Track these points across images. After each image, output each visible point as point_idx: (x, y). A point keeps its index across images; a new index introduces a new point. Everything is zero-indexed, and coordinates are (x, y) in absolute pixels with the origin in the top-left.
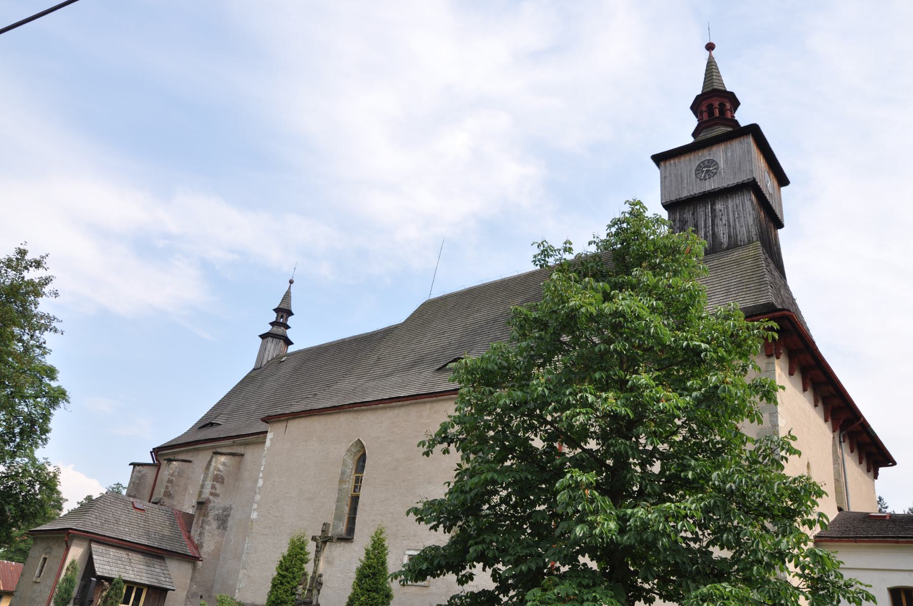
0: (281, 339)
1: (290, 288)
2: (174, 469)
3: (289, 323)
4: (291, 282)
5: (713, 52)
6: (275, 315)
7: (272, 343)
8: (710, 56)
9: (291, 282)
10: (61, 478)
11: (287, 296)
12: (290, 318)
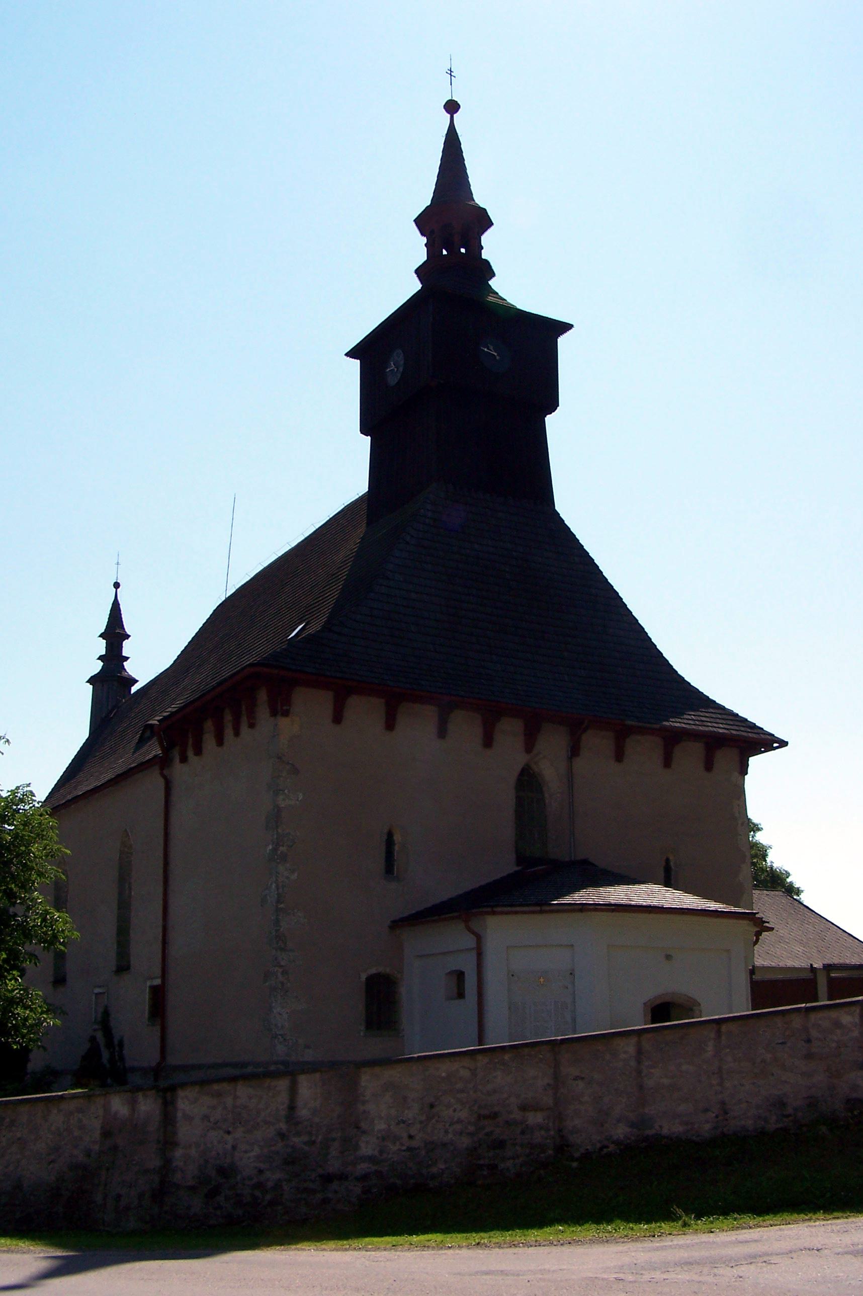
4: (117, 585)
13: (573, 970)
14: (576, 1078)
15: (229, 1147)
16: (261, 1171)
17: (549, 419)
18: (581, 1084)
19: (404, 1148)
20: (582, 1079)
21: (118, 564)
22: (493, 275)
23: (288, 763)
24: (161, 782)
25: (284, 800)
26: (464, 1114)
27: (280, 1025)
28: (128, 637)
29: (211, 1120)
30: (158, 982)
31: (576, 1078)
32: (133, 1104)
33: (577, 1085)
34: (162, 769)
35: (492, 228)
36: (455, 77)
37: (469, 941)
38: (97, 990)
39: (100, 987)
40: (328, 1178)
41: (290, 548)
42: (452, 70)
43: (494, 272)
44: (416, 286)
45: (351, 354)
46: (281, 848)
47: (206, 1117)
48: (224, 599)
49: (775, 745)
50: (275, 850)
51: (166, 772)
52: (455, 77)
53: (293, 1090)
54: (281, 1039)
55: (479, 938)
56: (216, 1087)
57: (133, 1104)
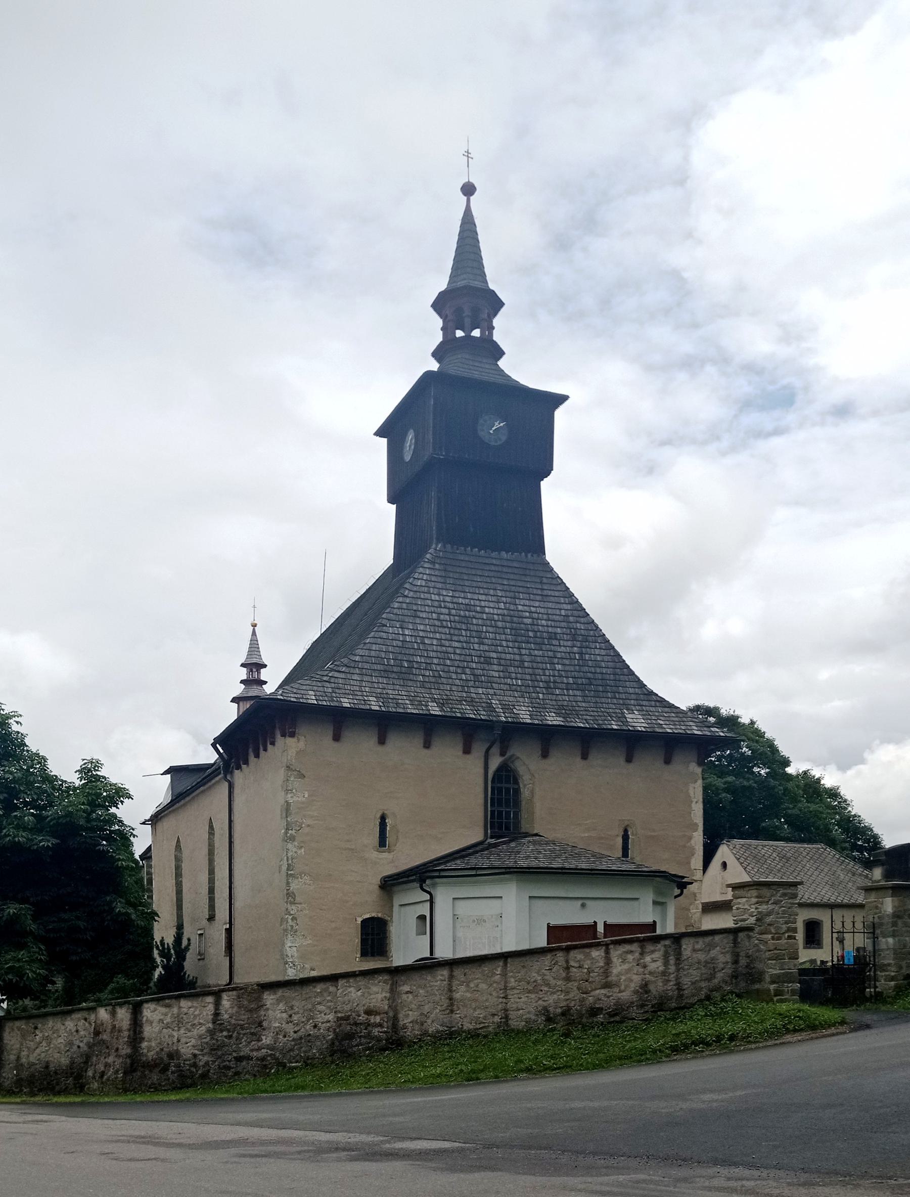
3: (263, 678)
5: (472, 198)
14: (407, 992)
15: (175, 1040)
16: (195, 1056)
17: (542, 482)
18: (411, 996)
19: (291, 1039)
20: (411, 993)
22: (501, 353)
23: (296, 770)
24: (226, 784)
25: (292, 797)
26: (331, 1017)
27: (290, 955)
29: (165, 1022)
30: (228, 926)
31: (407, 992)
32: (113, 1014)
33: (408, 997)
35: (431, 304)
36: (472, 158)
38: (199, 932)
40: (239, 1059)
41: (351, 603)
42: (469, 152)
43: (503, 351)
45: (380, 433)
46: (290, 832)
47: (161, 1021)
50: (286, 833)
52: (472, 158)
53: (217, 1004)
54: (291, 965)
56: (167, 1001)
57: (113, 1014)
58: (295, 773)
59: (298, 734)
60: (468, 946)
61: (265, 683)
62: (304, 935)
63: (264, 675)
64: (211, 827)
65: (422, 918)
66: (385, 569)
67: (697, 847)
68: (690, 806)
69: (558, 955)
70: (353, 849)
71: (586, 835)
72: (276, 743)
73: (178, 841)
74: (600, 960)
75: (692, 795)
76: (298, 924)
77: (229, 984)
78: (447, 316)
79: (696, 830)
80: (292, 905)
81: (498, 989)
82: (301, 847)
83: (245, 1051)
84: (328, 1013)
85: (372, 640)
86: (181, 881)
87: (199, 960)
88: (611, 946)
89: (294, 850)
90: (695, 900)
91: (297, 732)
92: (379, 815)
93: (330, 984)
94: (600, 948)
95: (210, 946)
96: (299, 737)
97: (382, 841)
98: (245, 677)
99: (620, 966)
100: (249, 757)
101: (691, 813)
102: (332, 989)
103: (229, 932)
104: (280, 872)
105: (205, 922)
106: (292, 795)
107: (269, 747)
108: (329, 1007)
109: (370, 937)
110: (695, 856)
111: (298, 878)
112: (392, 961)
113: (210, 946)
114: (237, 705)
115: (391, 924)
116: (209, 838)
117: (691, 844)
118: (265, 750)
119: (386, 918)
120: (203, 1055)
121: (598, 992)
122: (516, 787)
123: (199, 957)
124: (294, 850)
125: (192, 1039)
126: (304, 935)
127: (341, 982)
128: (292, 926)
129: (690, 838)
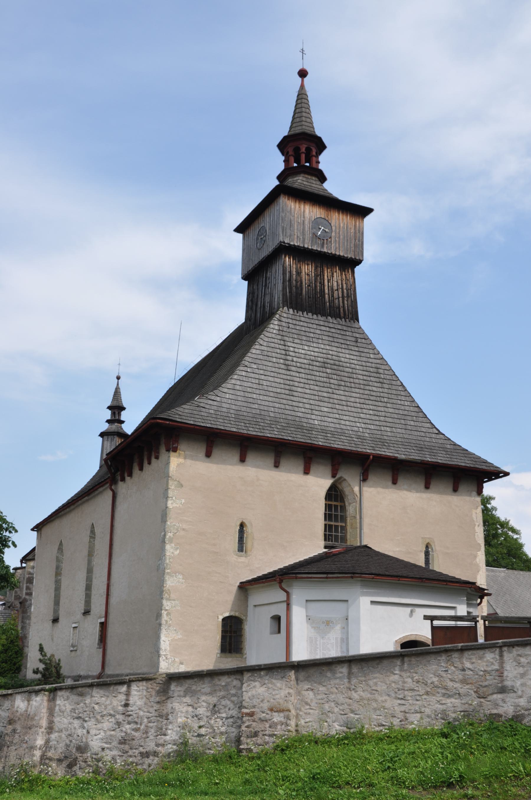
0: (115, 435)
1: (118, 384)
2: (19, 576)
3: (122, 418)
4: (118, 378)
5: (305, 79)
6: (109, 412)
7: (108, 440)
8: (302, 86)
9: (118, 378)
10: (525, 546)
11: (117, 393)
12: (123, 413)
13: (348, 616)
21: (119, 364)
24: (110, 493)
28: (124, 409)
29: (77, 711)
30: (103, 620)
34: (111, 485)
37: (283, 596)
38: (74, 625)
39: (75, 623)
44: (277, 183)
48: (173, 384)
49: (501, 475)
51: (113, 487)
53: (128, 694)
55: (288, 594)
56: (80, 689)
58: (176, 483)
59: (180, 449)
60: (318, 646)
61: (123, 422)
62: (175, 630)
63: (124, 415)
64: (93, 532)
65: (277, 619)
66: (231, 332)
67: (481, 565)
68: (474, 528)
69: (453, 656)
70: (218, 553)
71: (398, 549)
72: (160, 457)
73: (61, 544)
74: (494, 663)
75: (475, 519)
76: (171, 619)
77: (99, 676)
78: (288, 153)
79: (479, 550)
80: (168, 601)
81: (397, 690)
82: (177, 548)
83: (151, 746)
84: (231, 708)
85: (239, 377)
86: (60, 580)
87: (71, 651)
88: (505, 649)
89: (172, 550)
90: (482, 612)
91: (178, 448)
92: (239, 523)
93: (235, 677)
94: (494, 649)
95: (83, 639)
96: (180, 452)
97: (241, 546)
98: (109, 418)
99: (515, 669)
100: (133, 470)
101: (475, 535)
102: (236, 683)
103: (103, 626)
104: (158, 570)
105: (79, 616)
106: (172, 501)
107: (153, 460)
108: (233, 702)
109: (228, 634)
110: (480, 572)
111: (173, 576)
112: (246, 658)
113: (83, 639)
114: (102, 438)
115: (245, 623)
116: (90, 542)
117: (476, 562)
118: (149, 463)
119: (241, 617)
120: (110, 749)
121: (495, 696)
122: (342, 504)
123: (72, 649)
124: (172, 550)
125: (102, 731)
126: (175, 630)
127: (247, 676)
128: (166, 621)
129: (475, 556)
